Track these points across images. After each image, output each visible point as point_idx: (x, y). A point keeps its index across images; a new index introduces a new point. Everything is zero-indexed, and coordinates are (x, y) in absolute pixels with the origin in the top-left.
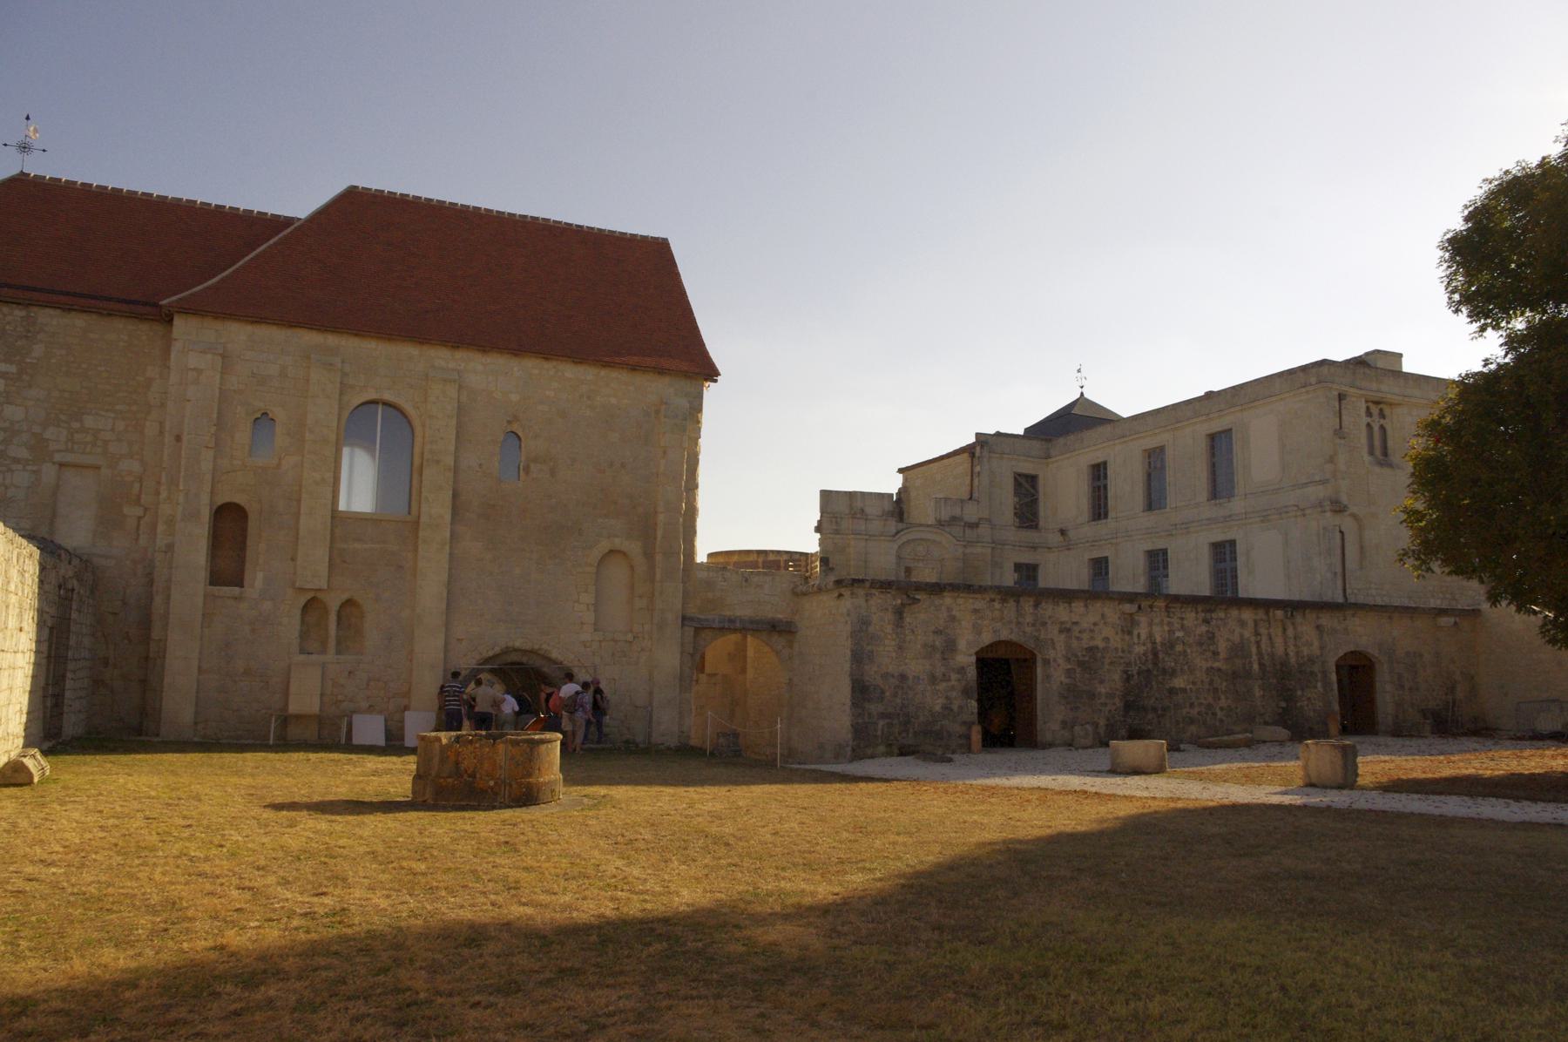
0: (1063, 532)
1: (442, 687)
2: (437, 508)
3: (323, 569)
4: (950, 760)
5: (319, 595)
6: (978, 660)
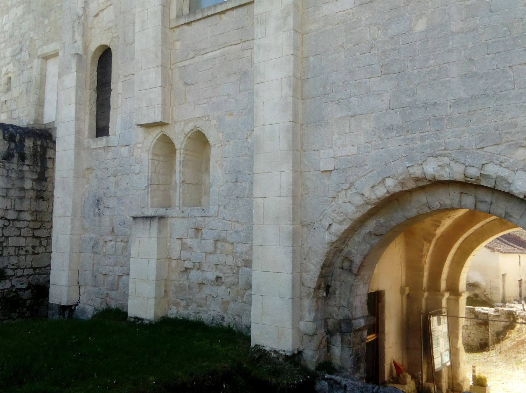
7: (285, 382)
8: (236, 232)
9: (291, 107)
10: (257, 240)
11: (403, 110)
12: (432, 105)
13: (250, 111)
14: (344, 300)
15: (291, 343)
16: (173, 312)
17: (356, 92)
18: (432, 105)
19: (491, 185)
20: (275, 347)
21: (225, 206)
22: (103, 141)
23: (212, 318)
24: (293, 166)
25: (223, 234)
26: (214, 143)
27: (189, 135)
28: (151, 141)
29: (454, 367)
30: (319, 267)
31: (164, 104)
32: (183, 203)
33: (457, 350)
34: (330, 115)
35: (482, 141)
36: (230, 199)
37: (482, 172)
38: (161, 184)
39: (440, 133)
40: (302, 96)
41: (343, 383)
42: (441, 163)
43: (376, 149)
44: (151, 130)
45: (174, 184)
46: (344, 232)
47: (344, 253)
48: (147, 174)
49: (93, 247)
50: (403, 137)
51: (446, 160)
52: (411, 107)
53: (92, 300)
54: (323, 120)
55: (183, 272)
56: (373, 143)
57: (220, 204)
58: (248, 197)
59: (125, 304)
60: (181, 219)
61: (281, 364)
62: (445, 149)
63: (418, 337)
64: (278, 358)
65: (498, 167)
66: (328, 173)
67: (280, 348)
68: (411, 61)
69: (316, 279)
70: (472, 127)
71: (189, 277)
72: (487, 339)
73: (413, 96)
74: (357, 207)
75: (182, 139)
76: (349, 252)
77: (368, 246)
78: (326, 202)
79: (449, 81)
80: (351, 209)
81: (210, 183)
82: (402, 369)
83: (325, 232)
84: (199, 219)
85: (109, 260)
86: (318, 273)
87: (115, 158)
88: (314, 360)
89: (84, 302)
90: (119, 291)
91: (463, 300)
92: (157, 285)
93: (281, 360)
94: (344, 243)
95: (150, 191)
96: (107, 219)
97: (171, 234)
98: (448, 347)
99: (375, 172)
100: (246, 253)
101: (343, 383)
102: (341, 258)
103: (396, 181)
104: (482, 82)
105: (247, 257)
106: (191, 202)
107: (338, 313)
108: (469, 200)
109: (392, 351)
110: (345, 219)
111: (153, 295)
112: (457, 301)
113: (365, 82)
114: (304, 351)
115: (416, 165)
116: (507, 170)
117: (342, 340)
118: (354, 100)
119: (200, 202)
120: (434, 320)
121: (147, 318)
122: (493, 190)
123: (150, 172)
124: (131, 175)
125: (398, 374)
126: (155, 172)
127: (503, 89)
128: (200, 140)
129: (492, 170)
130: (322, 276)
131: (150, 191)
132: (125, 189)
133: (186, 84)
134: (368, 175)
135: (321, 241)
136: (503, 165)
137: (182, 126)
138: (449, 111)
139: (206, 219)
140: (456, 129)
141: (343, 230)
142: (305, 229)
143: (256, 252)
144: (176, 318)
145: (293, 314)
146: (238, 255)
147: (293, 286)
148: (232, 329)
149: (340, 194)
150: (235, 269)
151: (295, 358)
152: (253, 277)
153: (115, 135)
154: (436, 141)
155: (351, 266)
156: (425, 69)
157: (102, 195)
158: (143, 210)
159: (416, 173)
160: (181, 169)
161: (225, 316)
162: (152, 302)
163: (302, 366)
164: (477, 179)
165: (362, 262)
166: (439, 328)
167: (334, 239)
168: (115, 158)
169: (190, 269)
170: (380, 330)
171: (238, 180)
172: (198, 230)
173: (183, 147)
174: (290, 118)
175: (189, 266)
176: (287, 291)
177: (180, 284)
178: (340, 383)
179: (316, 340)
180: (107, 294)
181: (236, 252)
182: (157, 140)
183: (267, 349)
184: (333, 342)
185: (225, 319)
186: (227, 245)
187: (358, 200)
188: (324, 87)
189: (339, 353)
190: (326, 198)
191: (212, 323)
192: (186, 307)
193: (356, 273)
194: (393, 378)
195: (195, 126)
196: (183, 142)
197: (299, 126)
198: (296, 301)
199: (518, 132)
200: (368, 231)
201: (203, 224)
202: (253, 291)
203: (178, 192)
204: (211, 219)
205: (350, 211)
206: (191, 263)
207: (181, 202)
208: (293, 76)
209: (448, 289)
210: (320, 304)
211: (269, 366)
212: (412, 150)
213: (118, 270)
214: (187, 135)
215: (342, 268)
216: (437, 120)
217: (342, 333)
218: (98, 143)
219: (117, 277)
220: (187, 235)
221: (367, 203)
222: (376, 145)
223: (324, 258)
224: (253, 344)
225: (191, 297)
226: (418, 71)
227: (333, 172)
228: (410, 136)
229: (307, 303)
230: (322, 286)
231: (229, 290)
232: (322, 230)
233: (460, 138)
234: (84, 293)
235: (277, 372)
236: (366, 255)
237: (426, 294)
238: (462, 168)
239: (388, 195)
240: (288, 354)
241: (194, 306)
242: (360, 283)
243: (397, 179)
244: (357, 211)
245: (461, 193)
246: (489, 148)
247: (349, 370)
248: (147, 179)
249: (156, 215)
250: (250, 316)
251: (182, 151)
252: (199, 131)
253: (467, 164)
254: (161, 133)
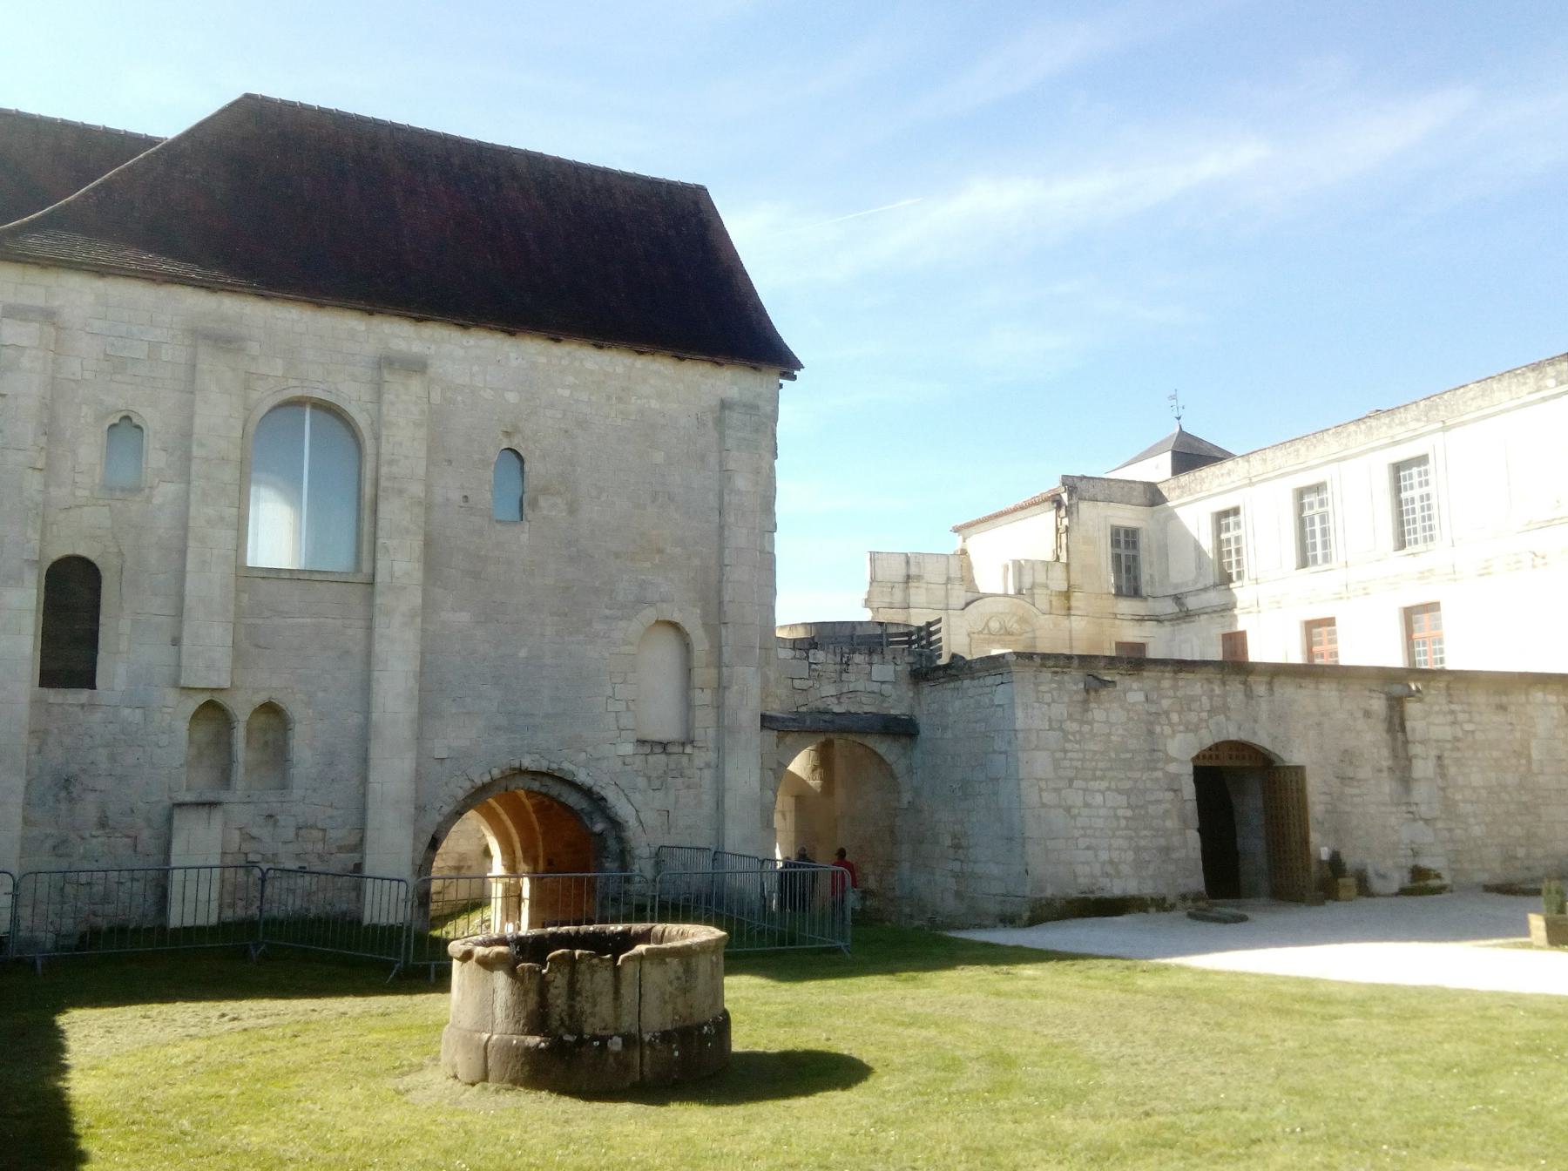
0: (1178, 599)
1: (1191, 916)
2: (401, 563)
3: (223, 658)
4: (1243, 919)
5: (218, 698)
6: (1196, 768)
8: (331, 817)
118: (469, 700)
129: (566, 766)
187: (468, 785)
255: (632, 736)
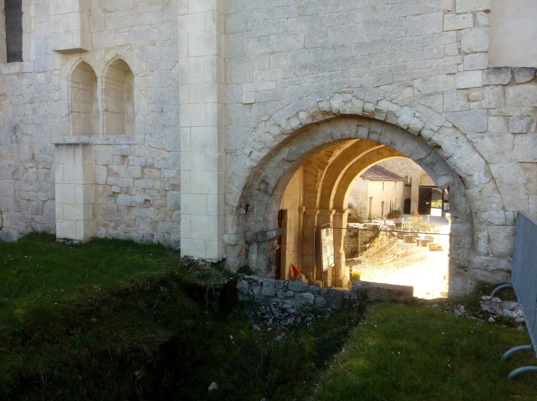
7: (212, 283)
8: (163, 159)
9: (215, 40)
10: (185, 165)
11: (316, 50)
12: (340, 47)
13: (174, 41)
14: (260, 216)
15: (216, 252)
16: (102, 233)
17: (276, 30)
18: (340, 47)
19: (382, 119)
20: (203, 256)
21: (151, 134)
22: (15, 67)
23: (142, 236)
24: (218, 98)
25: (150, 161)
26: (138, 72)
27: (110, 64)
28: (70, 67)
29: (336, 269)
30: (240, 189)
31: (83, 30)
32: (107, 131)
33: (340, 254)
34: (252, 51)
35: (378, 81)
36: (156, 128)
37: (377, 107)
38: (83, 111)
39: (346, 72)
40: (225, 31)
41: (260, 281)
42: (345, 99)
43: (292, 85)
44: (69, 56)
45: (94, 112)
46: (263, 158)
47: (261, 177)
48: (67, 101)
49: (13, 174)
50: (315, 75)
51: (349, 96)
52: (322, 48)
53: (16, 224)
54: (245, 55)
55: (111, 196)
56: (290, 79)
57: (146, 133)
58: (173, 126)
59: (51, 227)
60: (106, 147)
61: (208, 270)
62: (349, 87)
63: (311, 245)
64: (205, 265)
65: (389, 103)
66: (249, 106)
67: (207, 257)
68: (324, 5)
69: (238, 199)
70: (372, 68)
71: (117, 201)
72: (357, 248)
73: (325, 38)
74: (274, 137)
75: (104, 67)
76: (266, 176)
77: (282, 171)
78: (248, 132)
79: (355, 26)
80: (269, 138)
81: (133, 112)
82: (298, 271)
83: (246, 158)
84: (125, 146)
85: (31, 186)
86: (240, 194)
87: (31, 85)
88: (236, 265)
89: (8, 226)
90: (45, 215)
91: (345, 217)
92: (86, 209)
93: (208, 266)
94: (261, 168)
95: (71, 118)
96: (26, 146)
97: (96, 161)
98: (333, 252)
99: (290, 106)
100: (173, 178)
101: (260, 281)
102: (259, 181)
103: (308, 114)
104: (381, 28)
105: (175, 181)
106: (114, 130)
107: (256, 228)
108: (363, 132)
109: (290, 258)
110: (264, 147)
111: (82, 217)
112: (341, 216)
113: (284, 22)
114: (228, 258)
115: (325, 100)
116: (396, 105)
117: (258, 248)
118: (273, 38)
119: (123, 130)
120: (324, 232)
121: (77, 239)
122: (383, 123)
123: (70, 99)
124: (49, 102)
125: (295, 275)
126: (75, 99)
127: (398, 36)
128: (122, 69)
129: (384, 106)
130: (243, 197)
131: (71, 118)
132: (43, 116)
133: (105, 11)
134: (285, 108)
135: (243, 166)
136: (393, 101)
137: (103, 54)
138: (354, 53)
139: (132, 146)
140: (359, 69)
141: (262, 157)
142: (229, 156)
143: (184, 178)
144: (106, 238)
145: (219, 227)
146: (166, 179)
147: (219, 205)
148: (162, 245)
149: (260, 125)
150: (163, 192)
151: (219, 265)
152: (182, 198)
153: (29, 60)
154: (342, 79)
155: (267, 188)
156: (335, 14)
157: (19, 122)
158: (65, 137)
159: (325, 107)
160: (104, 97)
161: (155, 233)
162: (81, 224)
163: (225, 271)
164: (373, 113)
165: (276, 184)
166: (327, 238)
167: (254, 164)
168: (31, 85)
169: (118, 193)
170: (282, 242)
171: (164, 110)
172: (124, 157)
173: (104, 75)
174: (215, 52)
175: (116, 191)
176: (213, 210)
177: (108, 207)
178: (257, 282)
179: (237, 249)
180: (32, 219)
181: (164, 178)
182: (76, 67)
183: (196, 259)
184: (251, 250)
185: (155, 237)
186: (154, 171)
187: (276, 131)
188: (245, 24)
189: (256, 259)
190: (248, 128)
191: (142, 240)
192: (115, 228)
193: (271, 193)
194: (291, 278)
195: (117, 55)
196: (104, 70)
197: (222, 60)
198: (221, 216)
199: (407, 74)
200: (282, 158)
201: (129, 151)
202: (182, 210)
203: (101, 120)
204: (137, 146)
205: (268, 140)
206: (118, 188)
207: (105, 129)
208: (217, 10)
209: (334, 208)
210: (240, 220)
211: (198, 272)
212: (322, 87)
213: (42, 196)
214: (108, 63)
215: (259, 190)
216: (343, 61)
217: (258, 243)
218: (11, 68)
219: (41, 202)
220: (113, 161)
221: (283, 134)
222: (292, 82)
223: (245, 181)
224: (182, 255)
225: (119, 218)
226: (330, 15)
227: (254, 105)
228: (321, 74)
229: (230, 219)
230: (243, 205)
231: (157, 211)
232: (244, 157)
233: (361, 77)
234: (7, 218)
235: (205, 277)
236: (280, 179)
237: (318, 212)
238: (362, 103)
239: (300, 126)
240: (215, 262)
241: (123, 226)
242: (274, 202)
243: (309, 113)
244: (274, 141)
245: (358, 125)
246: (384, 87)
247: (263, 271)
248: (67, 107)
249: (79, 142)
250: (179, 232)
251: (104, 80)
252: (121, 60)
253: (366, 100)
254: (80, 61)
255: (481, 61)
